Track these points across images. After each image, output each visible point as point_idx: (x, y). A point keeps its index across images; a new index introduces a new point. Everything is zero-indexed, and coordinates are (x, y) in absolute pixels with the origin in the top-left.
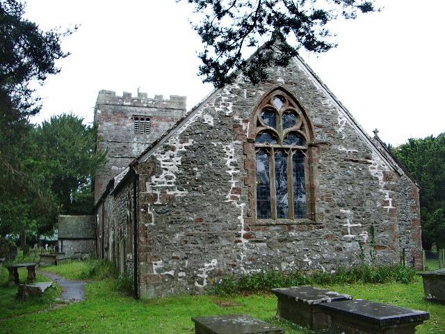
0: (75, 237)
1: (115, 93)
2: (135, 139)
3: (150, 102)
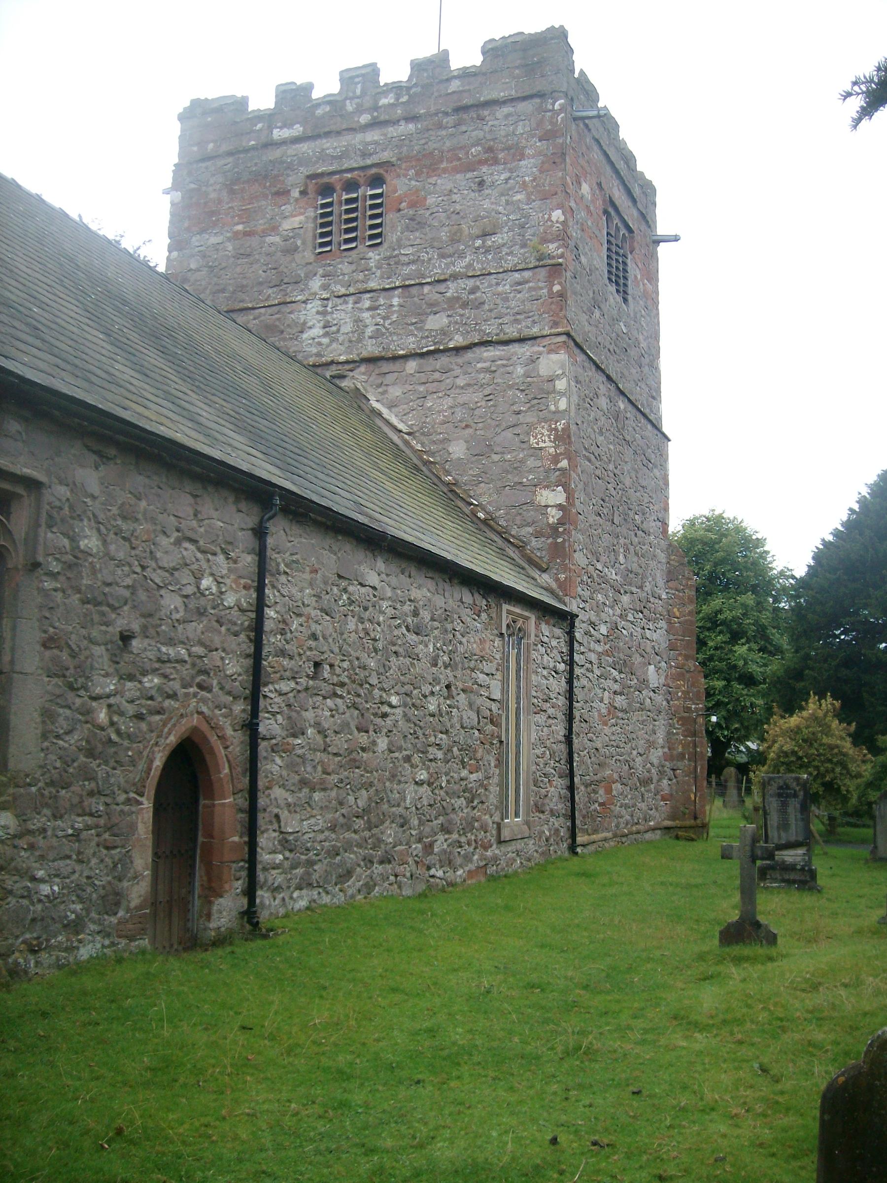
2: (316, 284)
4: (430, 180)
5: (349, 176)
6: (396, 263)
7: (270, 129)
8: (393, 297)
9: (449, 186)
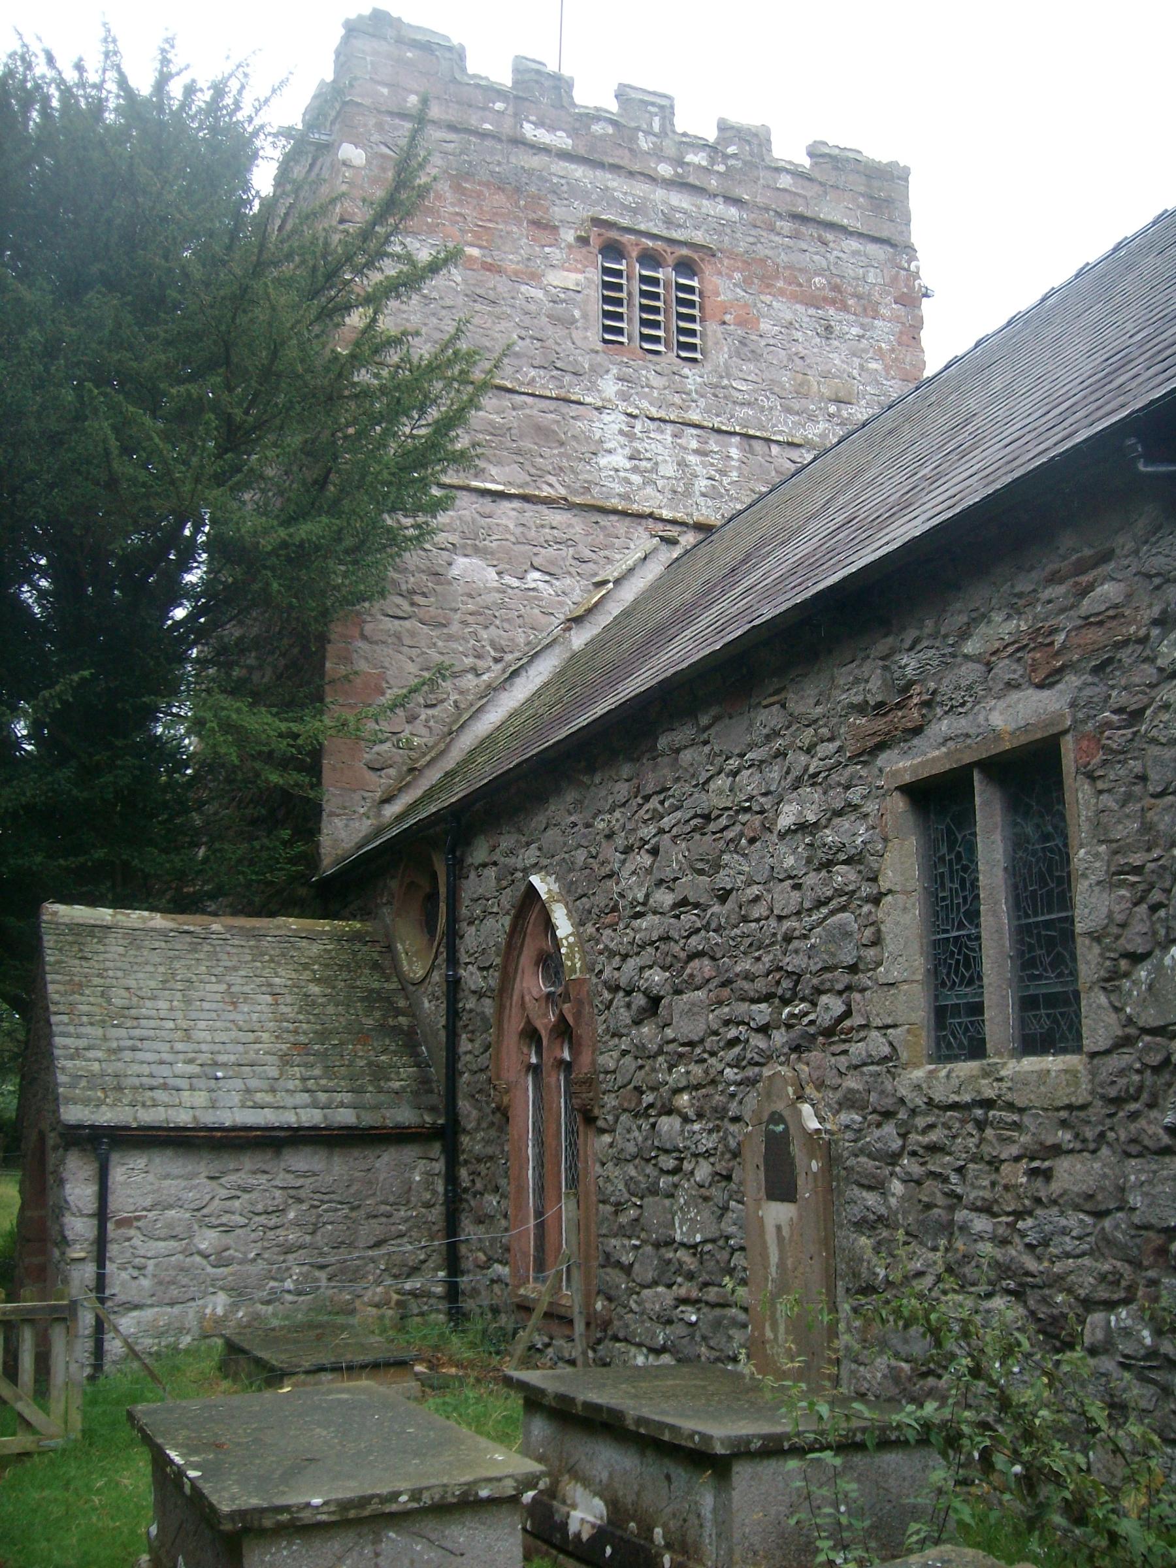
0: (234, 1115)
1: (667, 110)
2: (609, 387)
3: (697, 158)
4: (762, 297)
5: (650, 244)
6: (725, 397)
7: (518, 118)
8: (730, 445)
9: (789, 316)
